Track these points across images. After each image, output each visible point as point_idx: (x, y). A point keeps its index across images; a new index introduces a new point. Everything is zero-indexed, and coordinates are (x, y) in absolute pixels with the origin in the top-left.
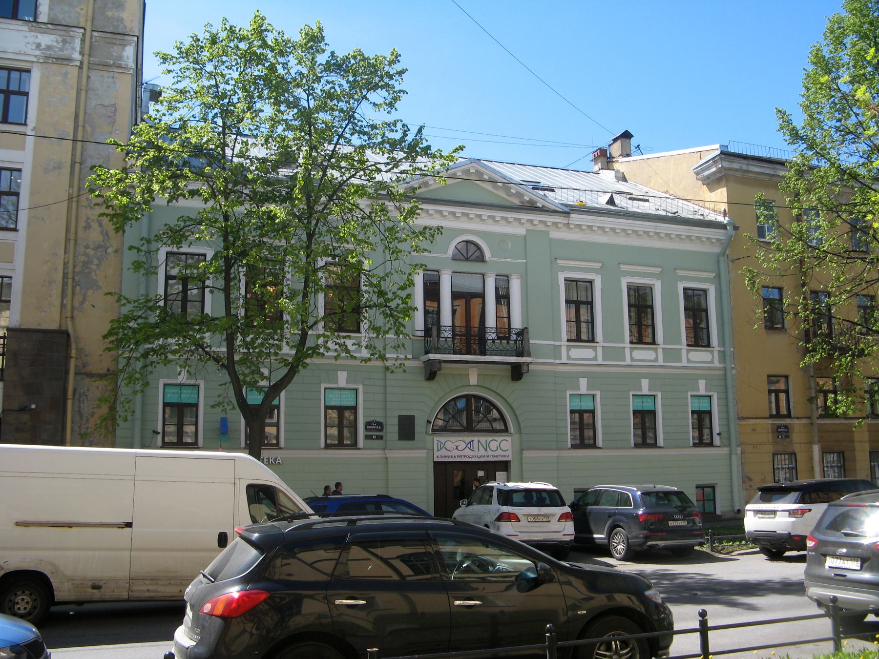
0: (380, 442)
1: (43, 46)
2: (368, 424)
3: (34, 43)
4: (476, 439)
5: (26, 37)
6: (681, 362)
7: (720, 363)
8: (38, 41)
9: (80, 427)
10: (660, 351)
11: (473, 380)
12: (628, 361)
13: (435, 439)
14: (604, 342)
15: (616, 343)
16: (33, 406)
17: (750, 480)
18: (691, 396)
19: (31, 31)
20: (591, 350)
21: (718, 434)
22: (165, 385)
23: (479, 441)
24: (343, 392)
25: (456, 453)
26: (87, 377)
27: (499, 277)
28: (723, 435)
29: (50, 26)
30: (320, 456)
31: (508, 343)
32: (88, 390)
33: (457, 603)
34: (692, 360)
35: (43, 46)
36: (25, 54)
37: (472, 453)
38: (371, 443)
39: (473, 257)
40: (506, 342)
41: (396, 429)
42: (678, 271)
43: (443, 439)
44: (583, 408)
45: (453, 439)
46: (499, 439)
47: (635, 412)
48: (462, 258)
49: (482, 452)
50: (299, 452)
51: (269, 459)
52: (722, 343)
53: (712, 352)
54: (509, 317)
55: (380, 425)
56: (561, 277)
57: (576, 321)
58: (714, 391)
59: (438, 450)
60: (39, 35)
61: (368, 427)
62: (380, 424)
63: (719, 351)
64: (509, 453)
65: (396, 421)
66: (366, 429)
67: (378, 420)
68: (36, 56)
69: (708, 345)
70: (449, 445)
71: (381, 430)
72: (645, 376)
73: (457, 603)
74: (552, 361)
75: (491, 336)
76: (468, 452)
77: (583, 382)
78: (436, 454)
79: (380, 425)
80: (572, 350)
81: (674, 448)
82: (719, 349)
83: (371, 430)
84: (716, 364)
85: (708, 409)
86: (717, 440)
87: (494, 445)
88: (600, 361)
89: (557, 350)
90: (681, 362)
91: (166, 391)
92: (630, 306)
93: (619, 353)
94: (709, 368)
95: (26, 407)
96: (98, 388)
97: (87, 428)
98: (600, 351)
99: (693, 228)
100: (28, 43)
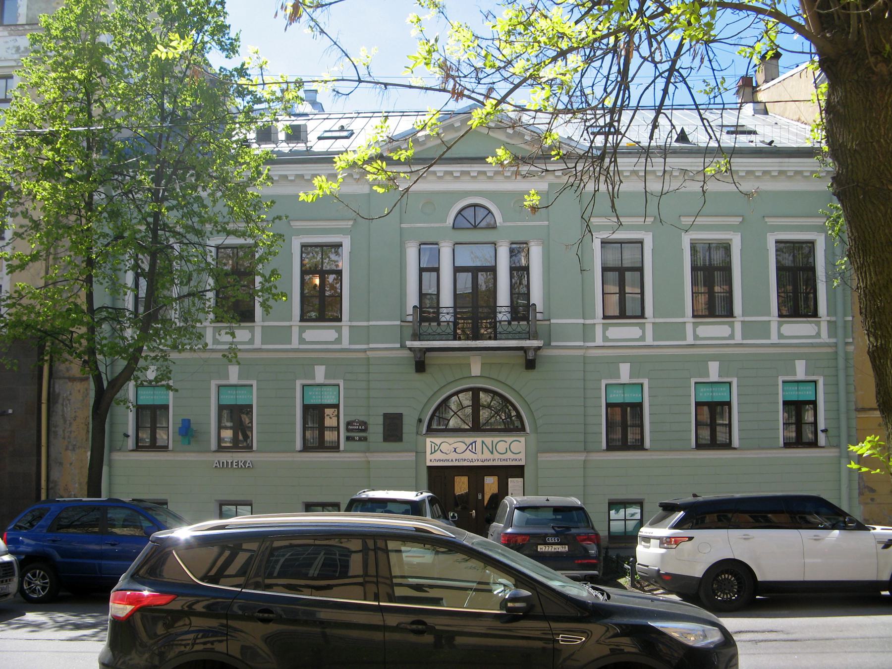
0: (363, 443)
1: (22, 49)
2: (348, 424)
3: (14, 47)
4: (479, 440)
5: (6, 42)
6: (769, 338)
7: (829, 337)
8: (17, 44)
9: (64, 431)
10: (649, 329)
11: (476, 370)
12: (690, 340)
13: (428, 440)
14: (743, 316)
15: (570, 318)
16: (10, 411)
17: (872, 490)
18: (783, 382)
19: (10, 35)
20: (247, 331)
21: (822, 431)
22: (303, 386)
23: (483, 442)
24: (324, 388)
25: (454, 456)
26: (70, 381)
27: (514, 246)
28: (830, 432)
29: (27, 27)
30: (295, 459)
31: (439, 325)
32: (70, 394)
33: (757, 597)
34: (701, 336)
35: (22, 49)
36: (6, 60)
37: (474, 456)
38: (352, 444)
39: (483, 224)
40: (435, 324)
41: (381, 429)
42: (767, 220)
43: (438, 441)
44: (801, 399)
45: (451, 440)
46: (509, 440)
47: (785, 403)
48: (469, 226)
49: (487, 455)
50: (271, 455)
51: (237, 462)
52: (831, 310)
53: (818, 324)
54: (438, 294)
55: (364, 427)
56: (686, 241)
57: (620, 293)
58: (818, 375)
59: (432, 453)
60: (18, 38)
61: (350, 427)
62: (364, 423)
63: (828, 322)
64: (522, 456)
65: (381, 420)
66: (348, 430)
67: (362, 419)
68: (15, 60)
69: (815, 314)
70: (444, 447)
71: (365, 430)
72: (714, 358)
73: (757, 597)
74: (581, 344)
75: (503, 316)
76: (468, 455)
77: (625, 370)
78: (429, 456)
79: (364, 427)
80: (611, 329)
81: (666, 450)
82: (828, 319)
83: (352, 430)
84: (825, 337)
85: (639, 401)
86: (822, 439)
87: (501, 447)
88: (649, 341)
89: (587, 332)
90: (769, 338)
91: (139, 392)
92: (694, 269)
93: (763, 329)
94: (812, 345)
95: (4, 412)
96: (79, 391)
97: (71, 432)
98: (738, 327)
99: (787, 160)
100: (9, 48)
